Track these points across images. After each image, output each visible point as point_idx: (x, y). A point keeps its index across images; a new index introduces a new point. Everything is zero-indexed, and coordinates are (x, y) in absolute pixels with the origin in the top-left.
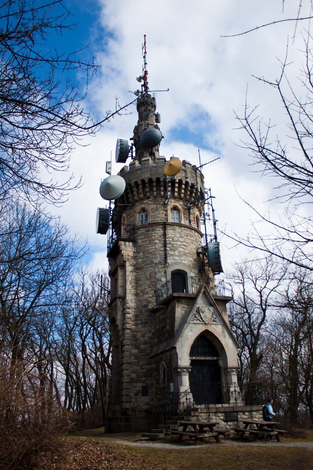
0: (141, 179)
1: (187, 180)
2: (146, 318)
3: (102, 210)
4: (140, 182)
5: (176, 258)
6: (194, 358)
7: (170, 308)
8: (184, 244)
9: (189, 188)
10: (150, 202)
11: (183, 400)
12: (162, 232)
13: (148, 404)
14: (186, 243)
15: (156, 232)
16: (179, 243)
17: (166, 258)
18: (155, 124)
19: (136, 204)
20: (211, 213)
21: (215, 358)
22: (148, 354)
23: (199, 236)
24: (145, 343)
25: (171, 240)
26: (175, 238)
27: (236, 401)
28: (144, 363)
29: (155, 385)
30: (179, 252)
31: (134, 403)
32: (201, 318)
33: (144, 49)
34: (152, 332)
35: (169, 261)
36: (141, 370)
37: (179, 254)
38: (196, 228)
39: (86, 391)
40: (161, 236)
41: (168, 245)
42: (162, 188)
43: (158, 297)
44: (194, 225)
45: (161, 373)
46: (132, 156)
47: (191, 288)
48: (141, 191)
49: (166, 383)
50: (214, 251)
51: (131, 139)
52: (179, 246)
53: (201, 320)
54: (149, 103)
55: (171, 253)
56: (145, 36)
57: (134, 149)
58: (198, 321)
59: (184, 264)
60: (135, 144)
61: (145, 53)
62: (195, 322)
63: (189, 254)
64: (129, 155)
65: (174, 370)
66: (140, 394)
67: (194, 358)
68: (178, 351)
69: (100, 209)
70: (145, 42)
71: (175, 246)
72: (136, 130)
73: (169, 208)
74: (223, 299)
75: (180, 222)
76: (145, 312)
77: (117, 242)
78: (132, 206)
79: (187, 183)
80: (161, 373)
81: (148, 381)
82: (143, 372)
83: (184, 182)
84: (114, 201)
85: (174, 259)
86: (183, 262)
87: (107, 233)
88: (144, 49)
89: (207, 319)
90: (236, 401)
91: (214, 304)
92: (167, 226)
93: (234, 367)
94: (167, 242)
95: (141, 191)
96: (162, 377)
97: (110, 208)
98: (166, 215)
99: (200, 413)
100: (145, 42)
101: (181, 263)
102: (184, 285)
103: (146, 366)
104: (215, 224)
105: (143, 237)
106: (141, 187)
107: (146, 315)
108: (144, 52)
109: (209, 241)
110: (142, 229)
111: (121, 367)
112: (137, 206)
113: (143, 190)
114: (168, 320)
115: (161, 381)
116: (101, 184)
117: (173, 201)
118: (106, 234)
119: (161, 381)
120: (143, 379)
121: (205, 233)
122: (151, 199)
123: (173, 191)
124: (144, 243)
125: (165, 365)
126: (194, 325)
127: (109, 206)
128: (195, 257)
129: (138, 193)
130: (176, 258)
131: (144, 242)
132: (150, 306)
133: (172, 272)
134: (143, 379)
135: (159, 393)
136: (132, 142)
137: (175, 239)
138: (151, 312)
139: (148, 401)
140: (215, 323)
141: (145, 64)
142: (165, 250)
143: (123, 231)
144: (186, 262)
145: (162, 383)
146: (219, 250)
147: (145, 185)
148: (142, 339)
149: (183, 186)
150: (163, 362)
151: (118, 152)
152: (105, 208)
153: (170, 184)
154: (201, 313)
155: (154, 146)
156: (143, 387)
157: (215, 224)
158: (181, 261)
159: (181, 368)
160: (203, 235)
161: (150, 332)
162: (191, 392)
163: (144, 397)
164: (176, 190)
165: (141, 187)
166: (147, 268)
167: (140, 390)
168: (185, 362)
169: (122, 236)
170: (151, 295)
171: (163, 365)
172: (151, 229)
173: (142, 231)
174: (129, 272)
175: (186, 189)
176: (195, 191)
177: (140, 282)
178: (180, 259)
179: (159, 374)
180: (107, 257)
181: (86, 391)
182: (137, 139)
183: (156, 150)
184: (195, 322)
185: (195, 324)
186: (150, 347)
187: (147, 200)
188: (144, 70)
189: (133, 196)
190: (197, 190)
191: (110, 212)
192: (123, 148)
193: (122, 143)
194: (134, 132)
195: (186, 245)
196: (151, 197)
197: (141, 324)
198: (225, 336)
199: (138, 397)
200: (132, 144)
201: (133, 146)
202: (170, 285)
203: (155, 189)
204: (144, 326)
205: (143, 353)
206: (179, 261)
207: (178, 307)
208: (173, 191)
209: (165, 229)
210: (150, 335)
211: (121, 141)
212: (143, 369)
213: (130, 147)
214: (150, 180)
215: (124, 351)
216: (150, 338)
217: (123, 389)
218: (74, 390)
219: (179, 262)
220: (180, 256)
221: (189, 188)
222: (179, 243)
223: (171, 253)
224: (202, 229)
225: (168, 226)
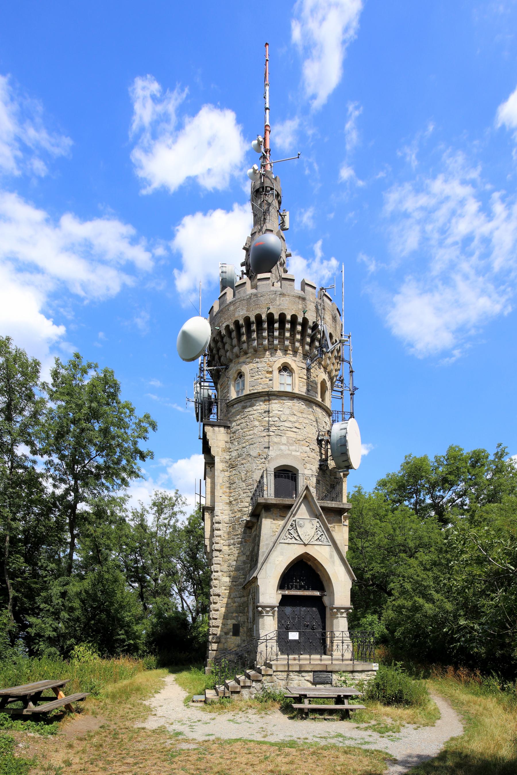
1: (306, 316)
5: (283, 447)
8: (297, 425)
10: (248, 360)
11: (261, 647)
13: (238, 646)
15: (255, 408)
16: (287, 424)
19: (230, 366)
25: (277, 419)
26: (283, 416)
27: (343, 657)
28: (236, 595)
31: (224, 644)
37: (287, 442)
53: (297, 538)
54: (269, 189)
59: (295, 457)
66: (231, 633)
68: (260, 582)
71: (281, 428)
75: (293, 389)
79: (305, 320)
83: (300, 320)
85: (280, 449)
89: (308, 537)
91: (321, 515)
93: (343, 606)
99: (274, 671)
101: (291, 454)
110: (236, 405)
120: (235, 615)
122: (250, 355)
124: (239, 427)
134: (235, 615)
137: (283, 418)
139: (240, 642)
140: (320, 543)
144: (298, 454)
149: (299, 328)
156: (234, 625)
158: (290, 452)
159: (264, 607)
161: (244, 554)
163: (235, 637)
164: (287, 334)
166: (242, 464)
168: (270, 597)
172: (248, 404)
174: (219, 471)
178: (289, 450)
187: (245, 357)
198: (333, 562)
214: (247, 320)
219: (288, 455)
220: (288, 444)
221: (309, 331)
222: (287, 424)
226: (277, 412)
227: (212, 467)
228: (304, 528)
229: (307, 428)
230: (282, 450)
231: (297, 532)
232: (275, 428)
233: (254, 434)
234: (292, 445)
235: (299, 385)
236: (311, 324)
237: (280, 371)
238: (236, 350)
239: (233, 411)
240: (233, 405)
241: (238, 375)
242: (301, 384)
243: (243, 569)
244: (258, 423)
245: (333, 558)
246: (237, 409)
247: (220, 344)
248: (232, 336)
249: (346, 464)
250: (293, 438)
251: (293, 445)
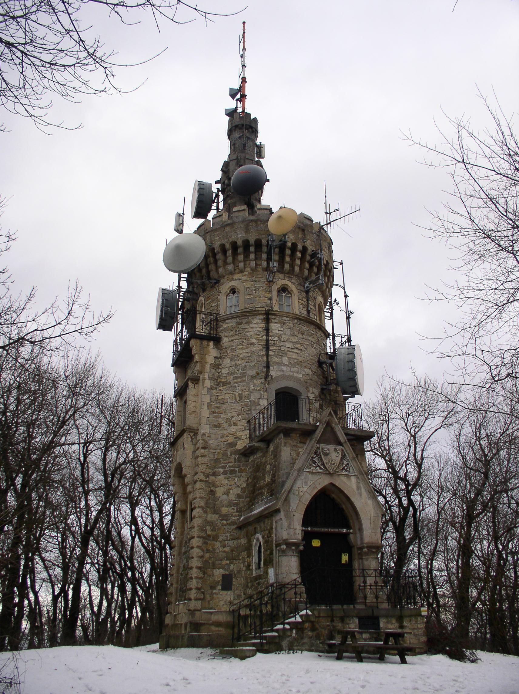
0: (231, 240)
1: (305, 244)
2: (232, 464)
3: (166, 292)
4: (228, 246)
5: (284, 368)
6: (309, 529)
7: (271, 448)
8: (298, 346)
9: (308, 258)
10: (244, 278)
12: (263, 325)
14: (302, 345)
15: (252, 326)
17: (268, 367)
18: (256, 159)
19: (222, 281)
20: (341, 300)
21: (344, 531)
22: (233, 523)
23: (323, 335)
24: (231, 504)
25: (277, 339)
26: (283, 336)
27: (377, 599)
29: (243, 573)
30: (289, 359)
32: (323, 464)
33: (242, 44)
34: (242, 486)
35: (273, 373)
36: (221, 549)
38: (318, 322)
39: (134, 591)
40: (260, 332)
41: (272, 348)
42: (264, 256)
43: (252, 430)
44: (314, 317)
45: (255, 552)
46: (218, 208)
47: (308, 416)
48: (230, 259)
49: (262, 569)
50: (347, 360)
51: (217, 182)
52: (289, 349)
55: (276, 360)
56: (244, 23)
57: (221, 197)
58: (318, 468)
59: (297, 380)
60: (223, 191)
61: (244, 49)
62: (313, 469)
63: (306, 364)
64: (213, 207)
65: (276, 547)
66: (219, 587)
67: (309, 529)
69: (163, 290)
70: (244, 33)
72: (226, 169)
73: (275, 288)
74: (360, 434)
76: (231, 454)
77: (188, 340)
78: (216, 283)
79: (305, 249)
80: (255, 552)
81: (232, 566)
82: (224, 552)
83: (300, 247)
84: (185, 275)
85: (281, 370)
86: (296, 375)
87: (173, 330)
88: (242, 44)
89: (333, 466)
90: (377, 599)
92: (270, 316)
94: (270, 342)
95: (230, 259)
96: (255, 559)
97: (179, 287)
98: (270, 299)
100: (244, 33)
102: (294, 415)
103: (231, 543)
104: (348, 318)
105: (231, 333)
106: (229, 253)
107: (233, 460)
108: (242, 47)
109: (338, 345)
110: (230, 321)
111: (189, 542)
112: (223, 283)
113: (234, 259)
114: (268, 467)
115: (254, 566)
116: (165, 246)
117: (281, 276)
118: (170, 329)
119: (254, 566)
121: (331, 332)
123: (281, 262)
125: (261, 540)
126: (310, 476)
127: (177, 285)
128: (315, 367)
129: (225, 263)
130: (284, 368)
131: (232, 341)
132: (240, 445)
133: (276, 391)
134: (224, 562)
135: (250, 585)
136: (219, 186)
137: (284, 337)
138: (241, 454)
141: (244, 66)
142: (268, 355)
143: (198, 323)
144: (301, 376)
145: (256, 569)
146: (354, 366)
147: (237, 250)
148: (225, 497)
149: (299, 255)
150: (259, 536)
151: (196, 195)
152: (171, 289)
153: (277, 250)
154: (323, 456)
155: (255, 192)
157: (348, 318)
158: (291, 374)
160: (329, 334)
161: (238, 486)
162: (304, 582)
163: (225, 592)
165: (229, 253)
167: (219, 582)
169: (197, 330)
170: (241, 427)
171: (258, 540)
172: (244, 321)
173: (230, 323)
175: (302, 259)
176: (317, 263)
177: (225, 406)
179: (249, 555)
180: (172, 366)
181: (134, 591)
182: (226, 182)
183: (256, 200)
184: (313, 469)
185: (313, 473)
186: (237, 512)
187: (240, 275)
188: (241, 76)
189: (217, 268)
190: (320, 260)
191: (179, 294)
192: (203, 195)
193: (202, 186)
194: (222, 170)
195: (301, 348)
196: (246, 269)
197: (225, 473)
198: (361, 495)
199: (214, 591)
200: (218, 189)
201: (220, 193)
202: (273, 410)
203: (252, 256)
204: (230, 477)
205: (226, 520)
206: (289, 373)
207: (285, 446)
208: (281, 262)
209: (267, 321)
210: (238, 491)
211: (201, 184)
212: (224, 546)
213: (214, 195)
215: (195, 517)
216: (239, 496)
217: (191, 578)
218: (116, 589)
219: (290, 376)
221: (308, 258)
222: (289, 345)
223: (276, 360)
224: (328, 326)
225: (273, 317)
226: (277, 332)
227: (197, 383)
228: (329, 456)
229: (308, 349)
230: (283, 371)
231: (322, 460)
232: (275, 348)
233: (252, 352)
234: (293, 366)
235: (299, 307)
236: (309, 251)
237: (279, 292)
238: (231, 267)
239: (225, 326)
240: (225, 320)
241: (230, 291)
242: (301, 306)
243: (237, 504)
244: (255, 341)
245: (361, 490)
246: (230, 325)
247: (211, 260)
248: (228, 255)
249: (353, 389)
250: (295, 359)
251: (295, 367)
